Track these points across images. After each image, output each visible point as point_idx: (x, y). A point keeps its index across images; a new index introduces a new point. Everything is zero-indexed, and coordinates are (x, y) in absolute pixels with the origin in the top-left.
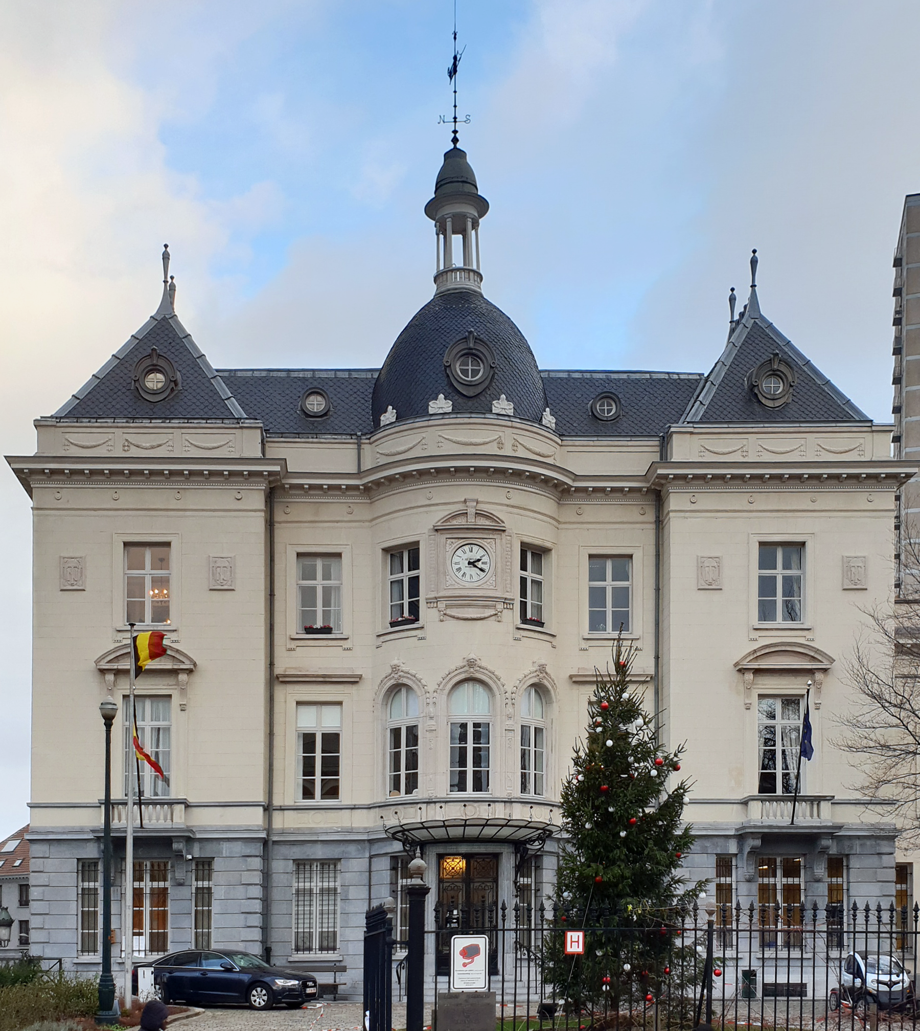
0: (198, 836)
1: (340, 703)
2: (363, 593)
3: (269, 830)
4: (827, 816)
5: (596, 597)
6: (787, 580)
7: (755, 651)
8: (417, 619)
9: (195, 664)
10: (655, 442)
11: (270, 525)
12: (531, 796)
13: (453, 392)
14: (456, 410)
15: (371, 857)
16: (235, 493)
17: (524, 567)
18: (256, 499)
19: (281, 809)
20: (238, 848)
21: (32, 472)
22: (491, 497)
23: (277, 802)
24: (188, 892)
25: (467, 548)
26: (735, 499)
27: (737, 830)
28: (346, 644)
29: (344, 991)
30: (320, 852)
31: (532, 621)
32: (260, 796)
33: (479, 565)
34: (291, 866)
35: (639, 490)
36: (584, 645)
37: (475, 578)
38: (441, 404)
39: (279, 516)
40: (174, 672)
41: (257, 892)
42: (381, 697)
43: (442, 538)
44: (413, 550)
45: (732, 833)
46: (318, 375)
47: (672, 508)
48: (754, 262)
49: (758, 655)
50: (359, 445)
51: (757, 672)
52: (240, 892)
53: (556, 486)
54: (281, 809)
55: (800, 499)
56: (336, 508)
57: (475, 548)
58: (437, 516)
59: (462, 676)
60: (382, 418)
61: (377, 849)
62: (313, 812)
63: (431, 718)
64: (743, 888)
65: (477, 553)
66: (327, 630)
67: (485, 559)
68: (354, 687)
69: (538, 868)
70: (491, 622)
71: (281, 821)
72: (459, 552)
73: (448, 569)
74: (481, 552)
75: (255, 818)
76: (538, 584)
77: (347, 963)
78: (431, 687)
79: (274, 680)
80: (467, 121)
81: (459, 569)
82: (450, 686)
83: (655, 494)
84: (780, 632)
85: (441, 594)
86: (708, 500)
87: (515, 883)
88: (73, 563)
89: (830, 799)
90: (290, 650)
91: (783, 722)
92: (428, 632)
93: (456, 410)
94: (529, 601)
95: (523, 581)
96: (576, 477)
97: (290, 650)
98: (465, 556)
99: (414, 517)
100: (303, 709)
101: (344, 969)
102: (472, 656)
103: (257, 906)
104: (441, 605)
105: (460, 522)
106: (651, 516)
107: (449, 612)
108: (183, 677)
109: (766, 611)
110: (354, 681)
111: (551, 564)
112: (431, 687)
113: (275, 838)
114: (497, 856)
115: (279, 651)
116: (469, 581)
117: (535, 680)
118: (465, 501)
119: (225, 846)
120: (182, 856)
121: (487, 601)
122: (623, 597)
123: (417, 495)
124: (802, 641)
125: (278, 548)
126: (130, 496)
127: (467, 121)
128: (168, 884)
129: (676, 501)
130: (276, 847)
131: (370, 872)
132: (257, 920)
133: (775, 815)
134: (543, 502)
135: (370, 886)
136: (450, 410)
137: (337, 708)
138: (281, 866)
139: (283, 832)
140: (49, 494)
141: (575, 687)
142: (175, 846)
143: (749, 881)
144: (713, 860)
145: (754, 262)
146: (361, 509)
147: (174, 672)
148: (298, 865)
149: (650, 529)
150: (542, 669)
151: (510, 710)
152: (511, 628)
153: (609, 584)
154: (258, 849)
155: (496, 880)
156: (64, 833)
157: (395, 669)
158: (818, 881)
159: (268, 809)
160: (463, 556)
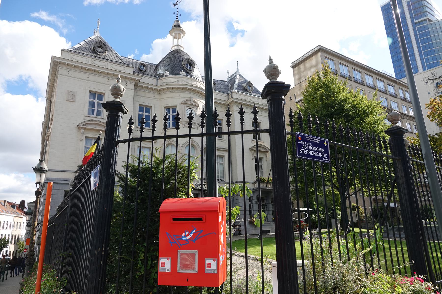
13: (185, 71)
26: (83, 75)
38: (182, 72)
48: (238, 63)
50: (157, 79)
51: (85, 129)
56: (151, 95)
58: (182, 100)
86: (72, 73)
105: (188, 102)
126: (92, 77)
127: (180, 15)
145: (238, 63)
156: (60, 181)
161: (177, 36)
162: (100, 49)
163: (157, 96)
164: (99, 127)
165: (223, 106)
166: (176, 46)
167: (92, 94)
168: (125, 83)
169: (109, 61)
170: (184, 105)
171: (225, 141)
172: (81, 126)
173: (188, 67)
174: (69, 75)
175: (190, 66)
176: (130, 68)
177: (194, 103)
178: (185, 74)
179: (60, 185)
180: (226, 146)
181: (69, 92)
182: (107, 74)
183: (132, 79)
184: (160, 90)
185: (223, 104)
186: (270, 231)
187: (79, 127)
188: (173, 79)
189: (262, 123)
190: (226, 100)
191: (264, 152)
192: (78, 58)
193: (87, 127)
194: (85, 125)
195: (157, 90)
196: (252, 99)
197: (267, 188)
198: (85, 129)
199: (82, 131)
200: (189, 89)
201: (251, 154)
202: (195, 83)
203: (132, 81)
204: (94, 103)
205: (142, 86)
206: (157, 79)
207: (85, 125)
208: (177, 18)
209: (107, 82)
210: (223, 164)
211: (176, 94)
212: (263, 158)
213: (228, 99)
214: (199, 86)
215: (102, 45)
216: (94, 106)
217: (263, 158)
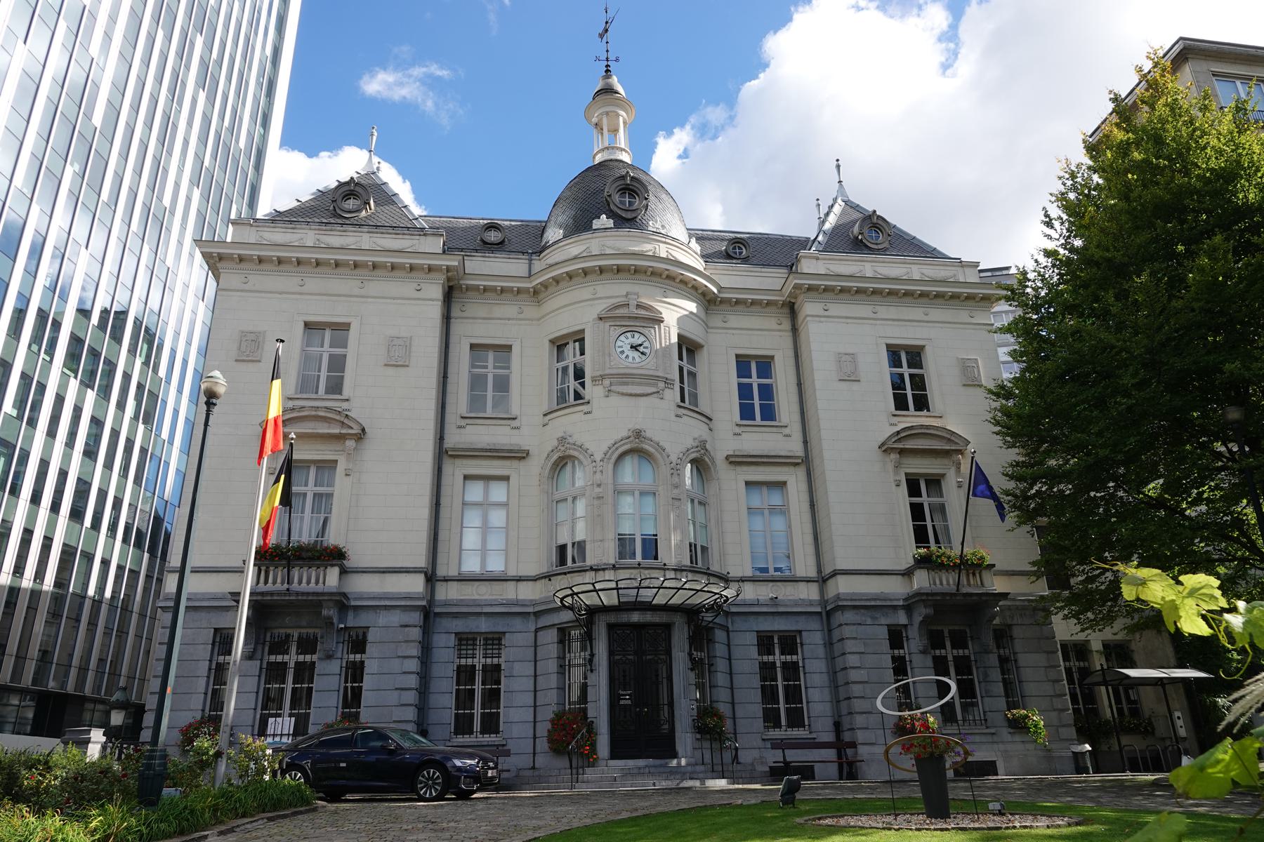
0: (353, 603)
1: (507, 478)
2: (532, 375)
3: (431, 601)
4: (998, 585)
5: (745, 391)
7: (898, 433)
9: (363, 430)
11: (447, 319)
13: (611, 215)
14: (617, 226)
15: (536, 631)
16: (415, 285)
17: (681, 358)
18: (435, 291)
19: (446, 580)
20: (396, 618)
21: (221, 257)
23: (441, 571)
24: (335, 666)
25: (629, 335)
26: (862, 309)
27: (905, 600)
28: (514, 423)
29: (508, 779)
30: (484, 626)
31: (688, 400)
32: (421, 561)
33: (641, 349)
34: (452, 640)
36: (738, 430)
37: (638, 360)
38: (604, 221)
39: (455, 312)
40: (340, 438)
41: (413, 665)
42: (550, 464)
45: (901, 603)
47: (809, 313)
48: (838, 167)
49: (899, 436)
51: (902, 452)
52: (396, 665)
53: (704, 294)
54: (446, 580)
56: (508, 309)
57: (637, 335)
58: (601, 307)
59: (627, 447)
61: (544, 621)
62: (477, 583)
63: (599, 486)
67: (646, 344)
68: (522, 463)
69: (711, 641)
70: (653, 400)
72: (622, 338)
74: (642, 339)
75: (416, 585)
76: (692, 375)
77: (511, 746)
78: (598, 457)
79: (442, 454)
80: (617, 60)
81: (622, 352)
82: (613, 460)
84: (913, 419)
85: (607, 372)
86: (837, 309)
87: (690, 654)
88: (252, 337)
90: (460, 427)
93: (617, 226)
94: (686, 386)
95: (681, 369)
97: (460, 427)
98: (627, 341)
100: (469, 484)
101: (507, 753)
103: (413, 681)
104: (607, 382)
106: (787, 325)
108: (350, 444)
109: (901, 403)
110: (520, 455)
111: (702, 358)
112: (598, 457)
113: (437, 610)
114: (668, 627)
115: (451, 419)
117: (693, 456)
118: (627, 294)
120: (332, 624)
122: (767, 392)
125: (453, 339)
126: (315, 283)
127: (617, 60)
128: (315, 657)
129: (809, 308)
130: (438, 620)
131: (536, 646)
132: (411, 697)
135: (536, 661)
137: (503, 485)
138: (444, 643)
139: (446, 604)
140: (232, 278)
141: (732, 467)
142: (325, 612)
144: (883, 633)
145: (838, 167)
147: (340, 438)
148: (460, 640)
149: (788, 336)
150: (702, 445)
151: (676, 479)
152: (673, 407)
153: (755, 381)
154: (416, 618)
155: (669, 652)
156: (203, 600)
158: (987, 652)
159: (431, 578)
160: (625, 342)
161: (605, 121)
162: (351, 204)
163: (531, 311)
164: (326, 425)
165: (772, 309)
166: (603, 150)
168: (415, 285)
169: (365, 229)
170: (607, 324)
171: (787, 431)
173: (623, 203)
174: (246, 287)
175: (631, 196)
176: (430, 239)
177: (643, 312)
178: (610, 223)
179: (203, 614)
180: (796, 447)
181: (243, 334)
182: (825, 290)
183: (431, 269)
184: (536, 292)
185: (769, 303)
186: (1000, 766)
188: (576, 247)
189: (928, 350)
191: (946, 454)
192: (308, 236)
193: (909, 445)
195: (526, 290)
196: (925, 271)
197: (964, 590)
198: (902, 452)
200: (619, 269)
201: (890, 467)
202: (647, 248)
203: (432, 275)
205: (476, 288)
207: (899, 440)
208: (607, 71)
209: (356, 291)
211: (582, 292)
212: (943, 475)
214: (664, 255)
215: (357, 189)
217: (943, 475)
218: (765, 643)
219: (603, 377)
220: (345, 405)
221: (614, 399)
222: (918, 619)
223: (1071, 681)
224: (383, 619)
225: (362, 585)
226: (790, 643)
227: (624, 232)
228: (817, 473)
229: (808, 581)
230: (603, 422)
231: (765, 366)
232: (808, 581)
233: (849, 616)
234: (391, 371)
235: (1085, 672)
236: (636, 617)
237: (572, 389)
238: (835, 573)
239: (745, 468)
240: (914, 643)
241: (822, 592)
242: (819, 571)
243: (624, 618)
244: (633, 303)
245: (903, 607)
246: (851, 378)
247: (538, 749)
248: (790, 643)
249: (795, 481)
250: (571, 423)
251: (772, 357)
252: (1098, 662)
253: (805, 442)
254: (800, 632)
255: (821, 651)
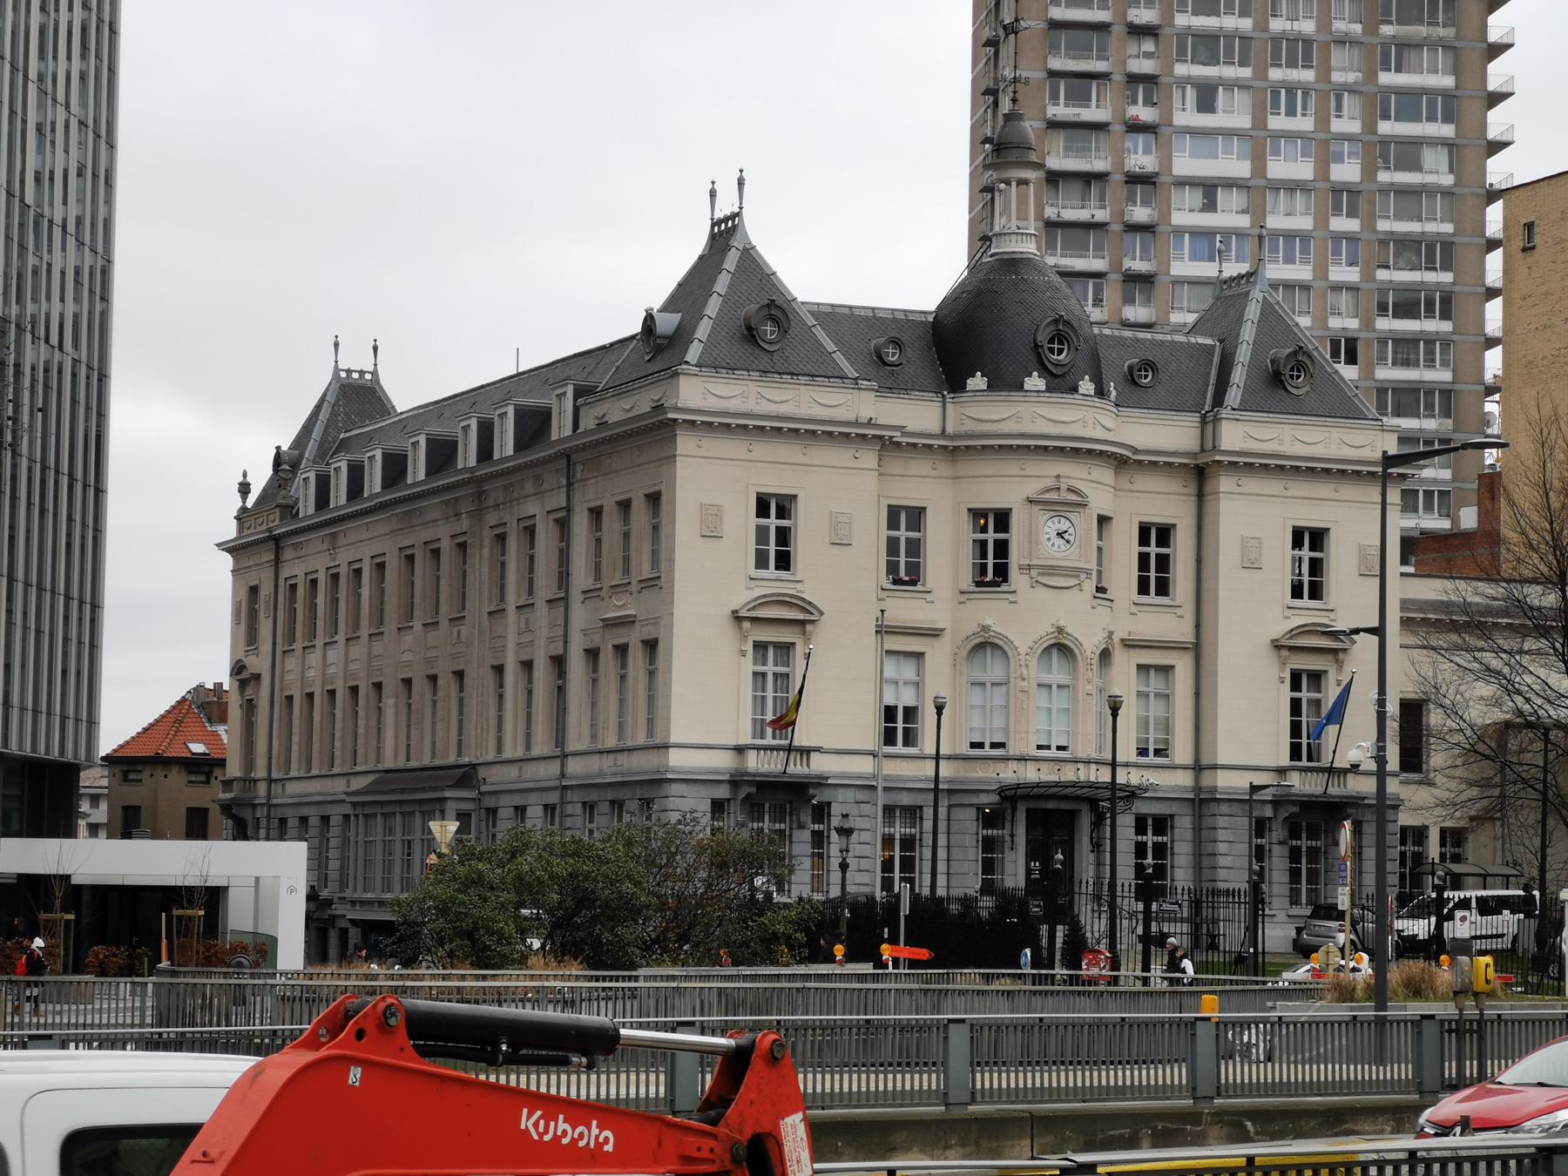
6: (1312, 560)
8: (1006, 580)
10: (1194, 419)
12: (1304, 763)
13: (1045, 371)
14: (1049, 389)
22: (1074, 473)
24: (806, 835)
26: (1273, 486)
28: (929, 597)
35: (1185, 465)
36: (1134, 609)
38: (1035, 382)
42: (969, 647)
43: (1035, 509)
44: (1002, 519)
46: (856, 312)
50: (944, 403)
51: (1292, 649)
55: (1325, 489)
58: (1032, 488)
60: (969, 381)
64: (1277, 850)
65: (1064, 525)
66: (913, 583)
70: (1074, 592)
71: (575, 766)
73: (1037, 538)
78: (1023, 650)
83: (1200, 473)
84: (1307, 613)
86: (1252, 484)
89: (818, 750)
91: (427, 534)
92: (1020, 596)
93: (1049, 389)
96: (1136, 451)
99: (1006, 487)
102: (1062, 623)
104: (1034, 573)
105: (1053, 496)
107: (1040, 579)
116: (1053, 550)
119: (841, 791)
121: (1072, 572)
122: (1163, 563)
123: (1011, 466)
124: (1326, 621)
126: (764, 450)
133: (1303, 784)
134: (1105, 474)
136: (1043, 388)
143: (1280, 843)
146: (944, 469)
149: (1192, 501)
152: (1090, 597)
157: (985, 628)
160: (1052, 527)
167: (977, 514)
172: (743, 613)
187: (737, 618)
190: (1197, 448)
194: (753, 609)
198: (755, 620)
199: (747, 625)
204: (984, 543)
206: (944, 403)
207: (753, 609)
209: (801, 459)
210: (1167, 696)
213: (1203, 450)
216: (984, 555)
217: (1325, 672)
218: (1140, 827)
219: (1030, 567)
220: (799, 586)
221: (1040, 590)
222: (1283, 814)
223: (1403, 864)
224: (842, 795)
225: (820, 765)
226: (1162, 824)
227: (1056, 397)
228: (1206, 661)
229: (1185, 768)
230: (1024, 615)
231: (1165, 534)
232: (1185, 768)
233: (1224, 808)
234: (836, 549)
235: (1419, 858)
236: (1051, 805)
237: (993, 568)
238: (1215, 767)
239: (1138, 651)
240: (1278, 833)
241: (1197, 779)
242: (1197, 760)
243: (1042, 805)
244: (1064, 487)
245: (1271, 802)
246: (1252, 566)
247: (1241, 912)
248: (1162, 824)
249: (1183, 666)
250: (991, 612)
251: (1174, 526)
252: (1433, 850)
253: (1198, 626)
254: (1172, 816)
255: (1189, 835)
